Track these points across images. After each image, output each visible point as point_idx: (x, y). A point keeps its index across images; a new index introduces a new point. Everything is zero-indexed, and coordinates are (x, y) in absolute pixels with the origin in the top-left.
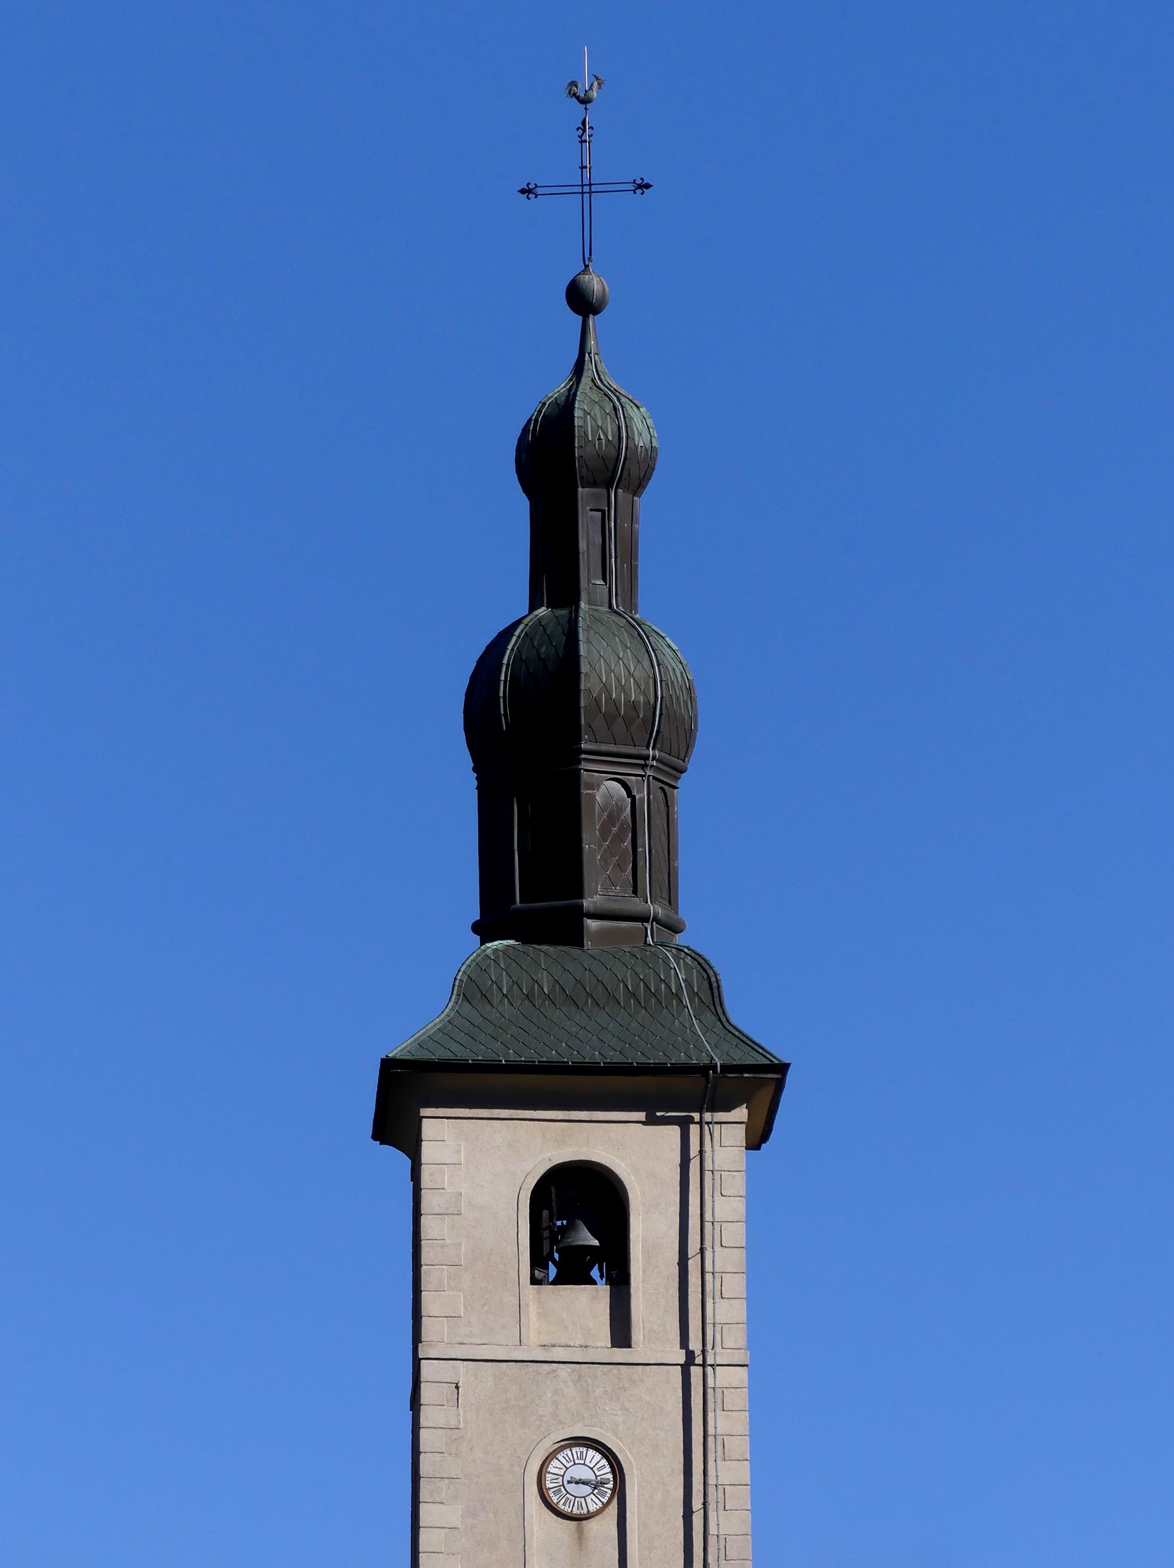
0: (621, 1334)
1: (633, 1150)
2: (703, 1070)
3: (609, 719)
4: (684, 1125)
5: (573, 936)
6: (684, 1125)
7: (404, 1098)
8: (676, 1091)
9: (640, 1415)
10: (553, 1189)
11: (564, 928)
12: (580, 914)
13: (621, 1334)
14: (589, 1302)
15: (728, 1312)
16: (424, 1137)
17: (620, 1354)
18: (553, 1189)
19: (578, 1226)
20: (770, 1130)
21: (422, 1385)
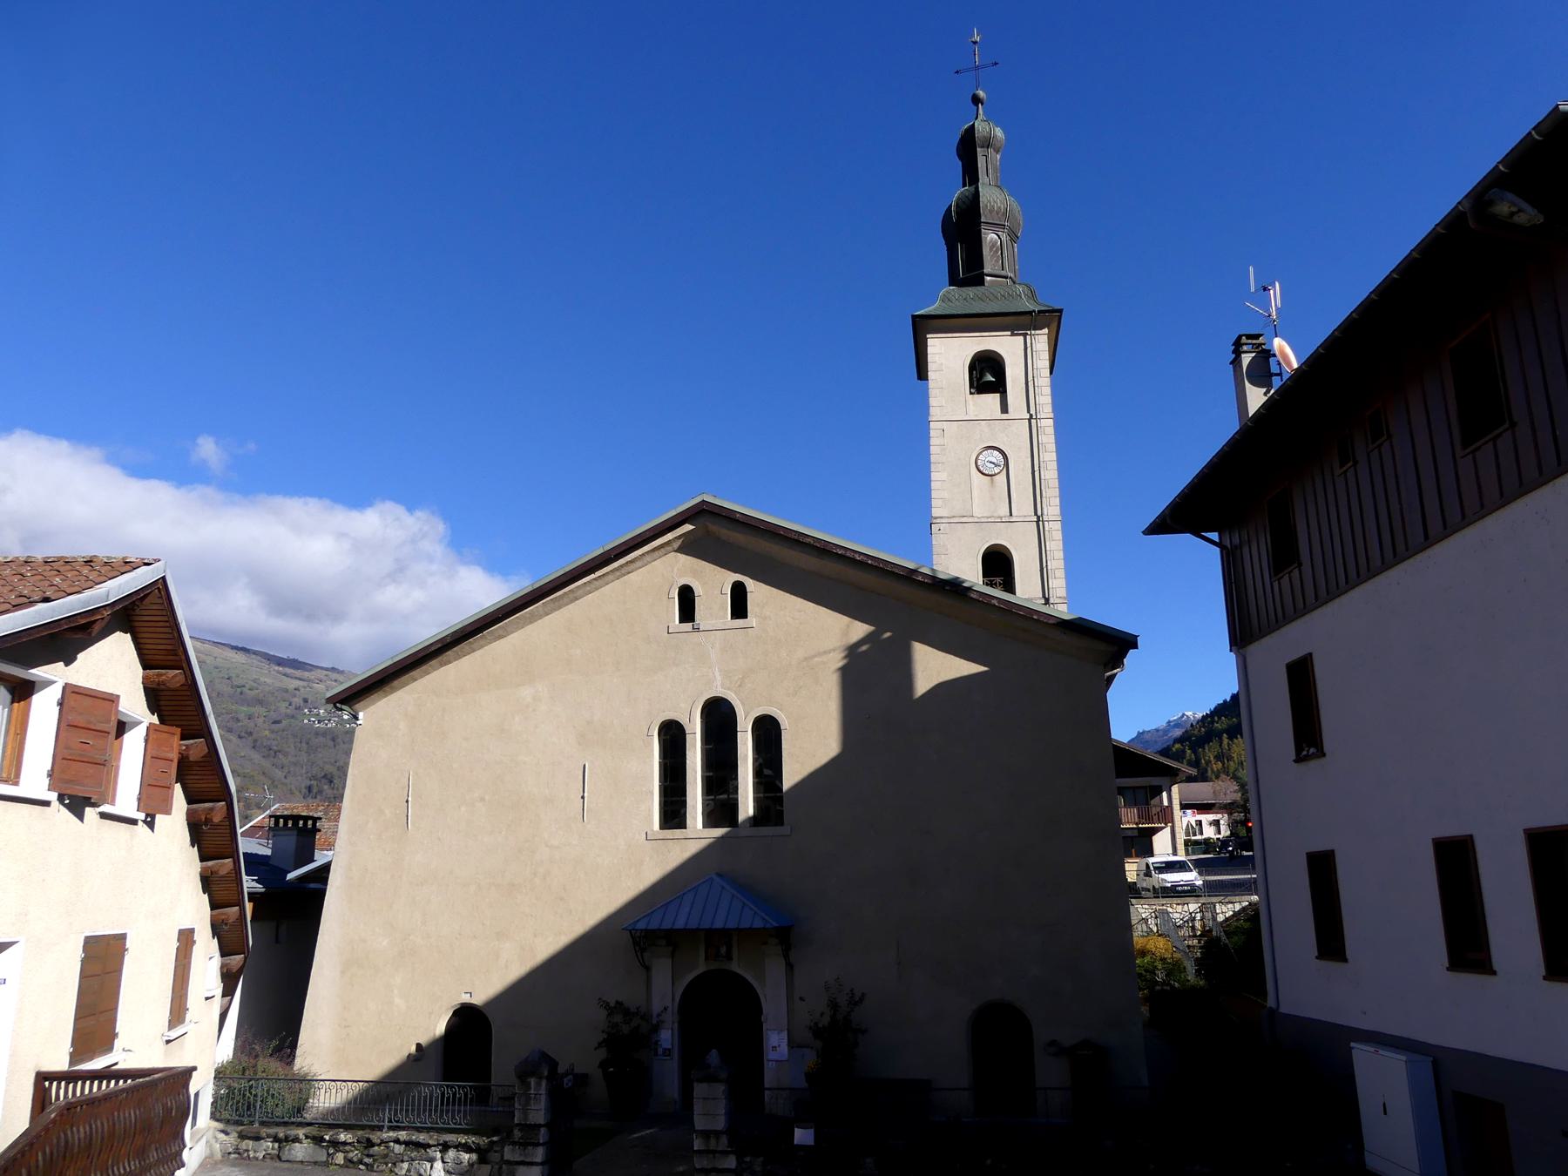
0: (1004, 409)
1: (1006, 345)
2: (1030, 313)
3: (991, 212)
4: (1025, 335)
5: (981, 282)
6: (1025, 335)
7: (923, 326)
8: (1019, 322)
9: (1014, 438)
10: (290, 876)
11: (978, 280)
12: (982, 275)
13: (1004, 409)
14: (993, 399)
15: (1044, 399)
16: (935, 413)
17: (1005, 416)
18: (290, 876)
19: (987, 374)
20: (295, 661)
21: (846, 619)
